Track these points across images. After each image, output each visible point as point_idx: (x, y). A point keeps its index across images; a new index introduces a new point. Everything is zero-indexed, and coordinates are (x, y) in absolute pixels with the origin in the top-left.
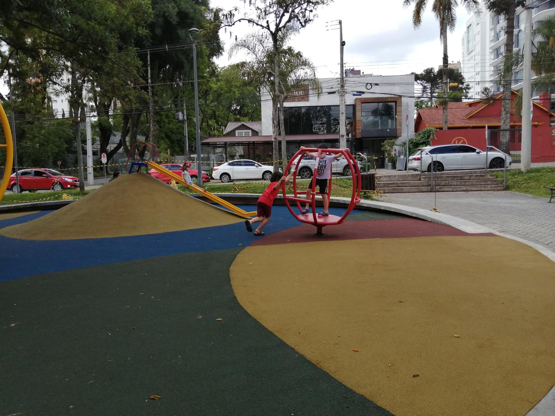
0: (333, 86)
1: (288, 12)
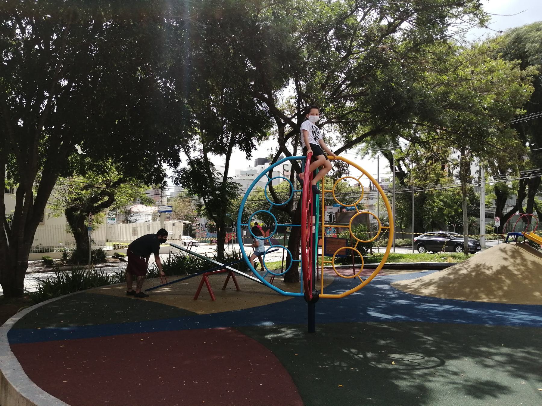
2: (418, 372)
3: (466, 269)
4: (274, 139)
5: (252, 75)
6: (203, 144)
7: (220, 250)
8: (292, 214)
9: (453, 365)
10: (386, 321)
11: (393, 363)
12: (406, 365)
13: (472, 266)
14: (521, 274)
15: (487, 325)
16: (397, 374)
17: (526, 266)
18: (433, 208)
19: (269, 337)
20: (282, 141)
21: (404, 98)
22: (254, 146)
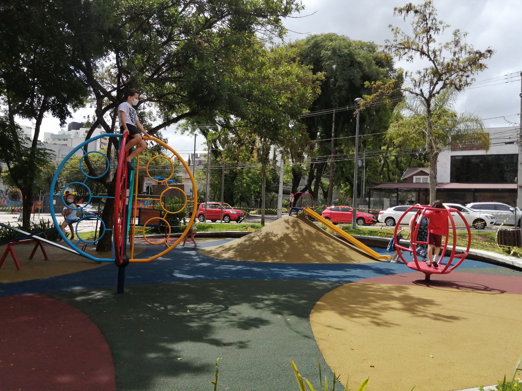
0: (511, 137)
1: (442, 80)
2: (206, 316)
3: (259, 236)
4: (91, 107)
5: (68, 39)
6: (9, 104)
7: (26, 219)
8: (107, 186)
9: (233, 309)
10: (188, 280)
11: (188, 311)
12: (198, 312)
13: (263, 234)
14: (297, 240)
15: (266, 280)
16: (190, 319)
17: (301, 233)
18: (242, 184)
19: (78, 299)
20: (100, 113)
21: (214, 91)
22: (69, 113)
